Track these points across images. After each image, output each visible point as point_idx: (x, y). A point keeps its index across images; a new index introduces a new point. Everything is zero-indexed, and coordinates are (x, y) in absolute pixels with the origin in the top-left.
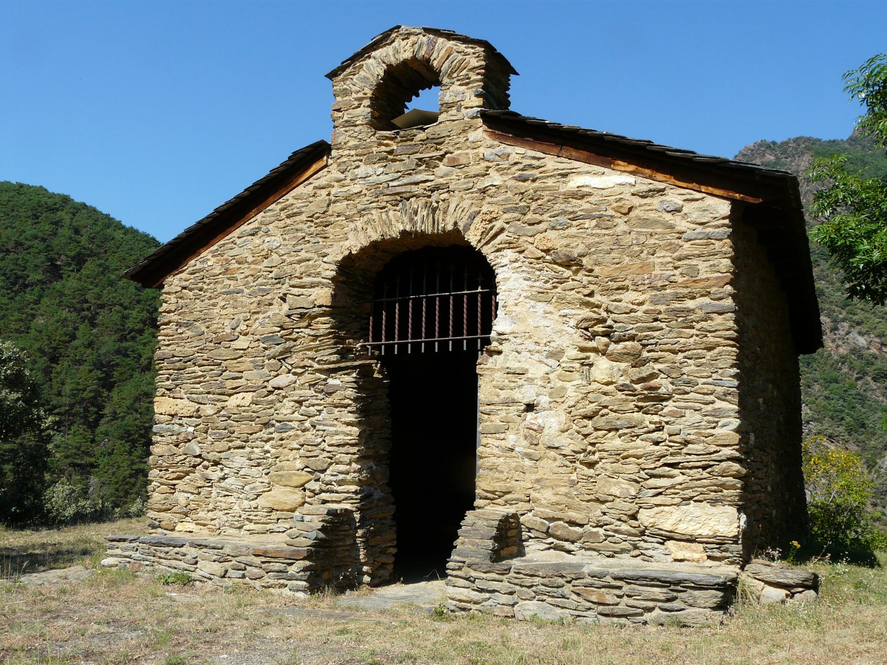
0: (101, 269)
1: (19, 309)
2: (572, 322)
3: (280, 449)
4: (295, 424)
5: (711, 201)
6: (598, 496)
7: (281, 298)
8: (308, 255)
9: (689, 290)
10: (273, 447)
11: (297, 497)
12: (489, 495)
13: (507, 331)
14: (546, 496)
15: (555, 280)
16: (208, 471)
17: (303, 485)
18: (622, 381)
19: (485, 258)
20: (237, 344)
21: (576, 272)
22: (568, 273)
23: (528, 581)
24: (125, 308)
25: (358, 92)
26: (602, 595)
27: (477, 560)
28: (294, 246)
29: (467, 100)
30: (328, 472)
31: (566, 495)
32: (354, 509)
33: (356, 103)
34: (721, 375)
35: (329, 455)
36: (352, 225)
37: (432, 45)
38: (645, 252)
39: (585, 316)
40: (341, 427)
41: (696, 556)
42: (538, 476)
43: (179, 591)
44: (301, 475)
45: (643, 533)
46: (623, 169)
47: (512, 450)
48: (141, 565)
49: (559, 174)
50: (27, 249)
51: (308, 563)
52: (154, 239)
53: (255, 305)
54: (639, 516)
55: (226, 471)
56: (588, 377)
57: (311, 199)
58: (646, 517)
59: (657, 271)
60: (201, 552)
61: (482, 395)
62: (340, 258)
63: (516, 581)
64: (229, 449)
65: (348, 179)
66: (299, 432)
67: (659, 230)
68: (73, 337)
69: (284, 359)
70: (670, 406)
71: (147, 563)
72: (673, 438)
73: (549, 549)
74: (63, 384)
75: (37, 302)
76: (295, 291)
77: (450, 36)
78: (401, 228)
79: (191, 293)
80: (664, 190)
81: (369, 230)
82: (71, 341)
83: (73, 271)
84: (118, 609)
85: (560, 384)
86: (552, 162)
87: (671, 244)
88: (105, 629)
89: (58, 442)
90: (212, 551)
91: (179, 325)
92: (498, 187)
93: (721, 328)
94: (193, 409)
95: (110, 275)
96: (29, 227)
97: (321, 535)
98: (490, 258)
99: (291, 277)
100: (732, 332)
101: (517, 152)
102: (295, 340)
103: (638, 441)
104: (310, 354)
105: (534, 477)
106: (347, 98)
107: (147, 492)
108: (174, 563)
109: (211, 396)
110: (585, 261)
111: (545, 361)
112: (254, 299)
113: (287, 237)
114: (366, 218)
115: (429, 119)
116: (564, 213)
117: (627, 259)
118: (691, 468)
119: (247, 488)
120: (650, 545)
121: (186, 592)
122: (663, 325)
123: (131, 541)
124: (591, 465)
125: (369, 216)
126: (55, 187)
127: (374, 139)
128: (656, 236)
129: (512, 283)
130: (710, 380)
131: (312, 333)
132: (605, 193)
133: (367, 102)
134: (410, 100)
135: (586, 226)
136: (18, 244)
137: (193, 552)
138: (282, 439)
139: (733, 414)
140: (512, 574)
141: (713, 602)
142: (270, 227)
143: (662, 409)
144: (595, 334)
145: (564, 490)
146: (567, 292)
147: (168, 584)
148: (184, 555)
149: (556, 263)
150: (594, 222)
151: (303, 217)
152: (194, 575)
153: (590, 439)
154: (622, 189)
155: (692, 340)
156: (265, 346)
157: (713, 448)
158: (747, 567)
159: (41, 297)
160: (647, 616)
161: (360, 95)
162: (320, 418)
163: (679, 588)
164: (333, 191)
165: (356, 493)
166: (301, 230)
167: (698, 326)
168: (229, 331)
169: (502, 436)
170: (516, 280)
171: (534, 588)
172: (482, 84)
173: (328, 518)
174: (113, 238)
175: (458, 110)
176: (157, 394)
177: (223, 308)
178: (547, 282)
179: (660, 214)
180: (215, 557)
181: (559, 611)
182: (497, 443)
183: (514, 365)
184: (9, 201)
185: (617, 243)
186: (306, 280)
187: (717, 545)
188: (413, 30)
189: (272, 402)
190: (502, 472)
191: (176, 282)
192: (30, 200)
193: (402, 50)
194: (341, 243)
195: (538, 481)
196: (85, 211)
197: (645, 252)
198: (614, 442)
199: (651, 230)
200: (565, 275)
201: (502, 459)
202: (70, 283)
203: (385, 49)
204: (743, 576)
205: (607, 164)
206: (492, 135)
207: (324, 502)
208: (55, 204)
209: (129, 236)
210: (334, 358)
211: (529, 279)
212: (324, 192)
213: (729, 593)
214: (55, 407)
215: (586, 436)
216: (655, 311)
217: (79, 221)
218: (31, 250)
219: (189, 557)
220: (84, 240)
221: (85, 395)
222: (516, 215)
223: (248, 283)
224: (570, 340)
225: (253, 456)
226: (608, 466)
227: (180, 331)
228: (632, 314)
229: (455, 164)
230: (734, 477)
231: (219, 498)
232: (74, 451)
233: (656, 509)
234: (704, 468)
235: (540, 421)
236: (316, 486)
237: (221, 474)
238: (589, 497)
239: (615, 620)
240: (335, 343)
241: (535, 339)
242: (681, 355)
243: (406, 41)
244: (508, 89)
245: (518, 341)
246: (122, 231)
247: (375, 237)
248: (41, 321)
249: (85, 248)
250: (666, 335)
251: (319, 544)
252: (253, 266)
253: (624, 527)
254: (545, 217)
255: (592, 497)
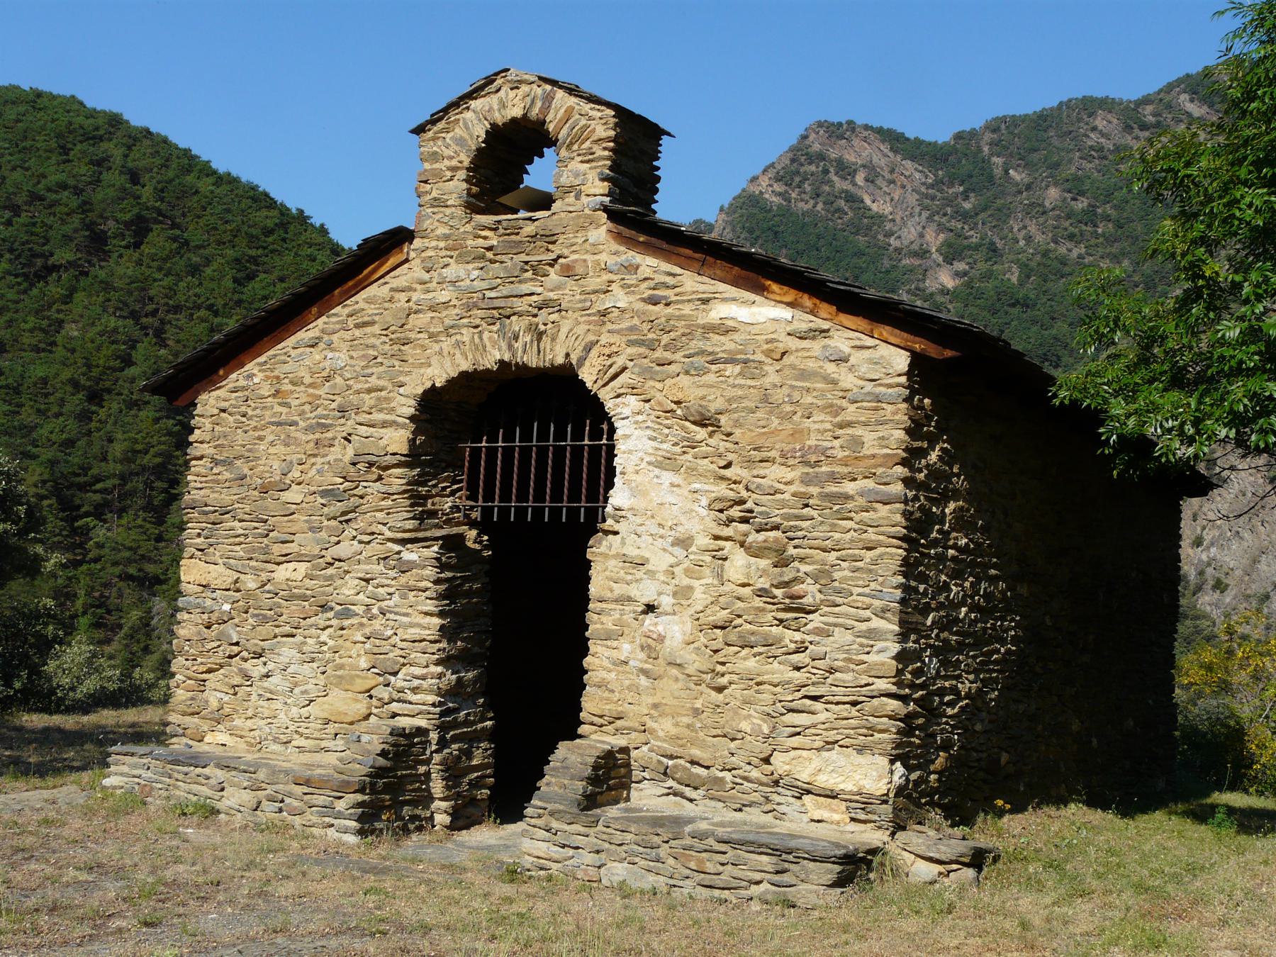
0: (175, 245)
1: (37, 312)
2: (704, 502)
3: (341, 641)
4: (359, 609)
5: (885, 351)
6: (727, 730)
7: (346, 439)
8: (381, 383)
9: (850, 469)
10: (330, 637)
11: (361, 707)
12: (596, 720)
13: (625, 506)
14: (664, 727)
15: (685, 443)
16: (247, 665)
17: (369, 691)
18: (763, 583)
19: (602, 405)
20: (287, 496)
21: (711, 435)
22: (701, 433)
23: (619, 837)
24: (216, 314)
25: (451, 158)
26: (701, 861)
27: (561, 807)
28: (363, 368)
29: (589, 184)
30: (400, 675)
31: (688, 726)
32: (430, 727)
33: (449, 174)
34: (881, 584)
35: (401, 653)
36: (436, 347)
37: (548, 99)
38: (799, 414)
39: (719, 495)
40: (419, 618)
41: (836, 817)
42: (656, 701)
43: (199, 826)
44: (366, 678)
45: (776, 783)
46: (778, 298)
47: (626, 663)
48: (152, 789)
49: (699, 299)
50: (51, 206)
51: (360, 797)
52: (266, 195)
53: (312, 444)
54: (772, 760)
55: (271, 666)
56: (720, 576)
57: (386, 305)
58: (780, 763)
59: (812, 442)
60: (228, 775)
61: (593, 589)
62: (420, 391)
63: (605, 837)
64: (275, 637)
65: (435, 281)
66: (364, 621)
67: (819, 385)
68: (128, 362)
69: (347, 521)
70: (816, 620)
71: (160, 786)
72: (817, 663)
73: (668, 794)
74: (110, 441)
75: (67, 299)
76: (363, 430)
77: (573, 91)
78: (498, 357)
79: (231, 419)
80: (828, 331)
81: (458, 355)
82: (122, 370)
83: (127, 247)
84: (108, 851)
85: (686, 581)
86: (691, 282)
87: (831, 406)
88: (83, 876)
89: (101, 539)
90: (242, 776)
91: (216, 462)
92: (623, 311)
93: (885, 522)
94: (230, 580)
95: (191, 255)
96: (52, 169)
97: (382, 762)
98: (609, 405)
99: (358, 410)
100: (899, 528)
101: (649, 264)
102: (361, 497)
103: (776, 664)
104: (380, 515)
105: (650, 700)
106: (437, 166)
107: (169, 689)
108: (195, 788)
109: (253, 563)
110: (723, 420)
111: (670, 549)
112: (312, 437)
113: (354, 354)
114: (454, 338)
115: (543, 201)
116: (702, 352)
117: (776, 421)
118: (837, 703)
119: (297, 691)
120: (785, 800)
121: (207, 828)
122: (815, 513)
123: (142, 756)
124: (720, 689)
125: (458, 337)
126: (98, 99)
127: (469, 228)
128: (815, 394)
129: (634, 441)
130: (867, 590)
131: (384, 489)
132: (755, 330)
133: (462, 174)
134: (531, 162)
135: (727, 373)
136: (35, 197)
137: (220, 774)
138: (342, 629)
139: (890, 636)
140: (600, 827)
141: (832, 877)
142: (335, 337)
143: (806, 624)
144: (731, 520)
145: (686, 720)
146: (699, 461)
147: (185, 814)
148: (208, 778)
149: (686, 420)
150: (738, 369)
151: (376, 329)
152: (219, 805)
153: (719, 657)
154: (777, 326)
155: (849, 536)
156: (323, 501)
157: (864, 679)
158: (899, 835)
159: (73, 290)
160: (755, 890)
161: (454, 163)
162: (391, 603)
163: (790, 858)
164: (415, 296)
165: (433, 705)
166: (373, 347)
167: (857, 517)
168: (278, 478)
169: (615, 644)
170: (638, 438)
171: (624, 847)
172: (609, 163)
173: (390, 739)
174: (197, 192)
175: (577, 197)
176: (185, 555)
177: (272, 444)
178: (676, 444)
179: (821, 363)
180: (246, 784)
181: (651, 878)
182: (608, 653)
183: (631, 551)
184: (18, 121)
185: (765, 399)
186: (378, 417)
187: (862, 805)
188: (526, 77)
189: (331, 578)
190: (613, 691)
191: (212, 402)
192: (53, 121)
193: (510, 104)
194: (422, 371)
195: (655, 706)
196: (147, 142)
197: (799, 414)
198: (748, 663)
199: (808, 385)
200: (698, 437)
201: (613, 675)
202: (122, 267)
203: (487, 99)
204: (892, 848)
205: (760, 289)
206: (619, 237)
207: (394, 715)
208: (97, 129)
209: (223, 189)
210: (410, 524)
211: (654, 439)
212: (403, 297)
213: (854, 867)
214: (98, 479)
215: (716, 651)
216: (805, 493)
217: (138, 160)
218: (58, 209)
219: (213, 782)
220: (147, 193)
221: (147, 460)
222: (642, 350)
223: (303, 412)
224: (700, 524)
225: (305, 649)
226: (738, 694)
227: (215, 471)
228: (778, 496)
229: (568, 272)
230: (890, 717)
231: (261, 703)
232: (127, 554)
233: (793, 753)
234: (854, 704)
235: (660, 628)
236: (384, 693)
237: (264, 670)
238: (715, 732)
239: (717, 893)
240: (412, 505)
241: (659, 520)
242: (834, 554)
243: (515, 91)
244: (658, 159)
245: (639, 521)
246: (211, 180)
247: (465, 366)
248: (72, 330)
249: (148, 209)
250: (816, 526)
251: (378, 772)
252: (311, 391)
253: (755, 774)
254: (678, 356)
255: (719, 732)
